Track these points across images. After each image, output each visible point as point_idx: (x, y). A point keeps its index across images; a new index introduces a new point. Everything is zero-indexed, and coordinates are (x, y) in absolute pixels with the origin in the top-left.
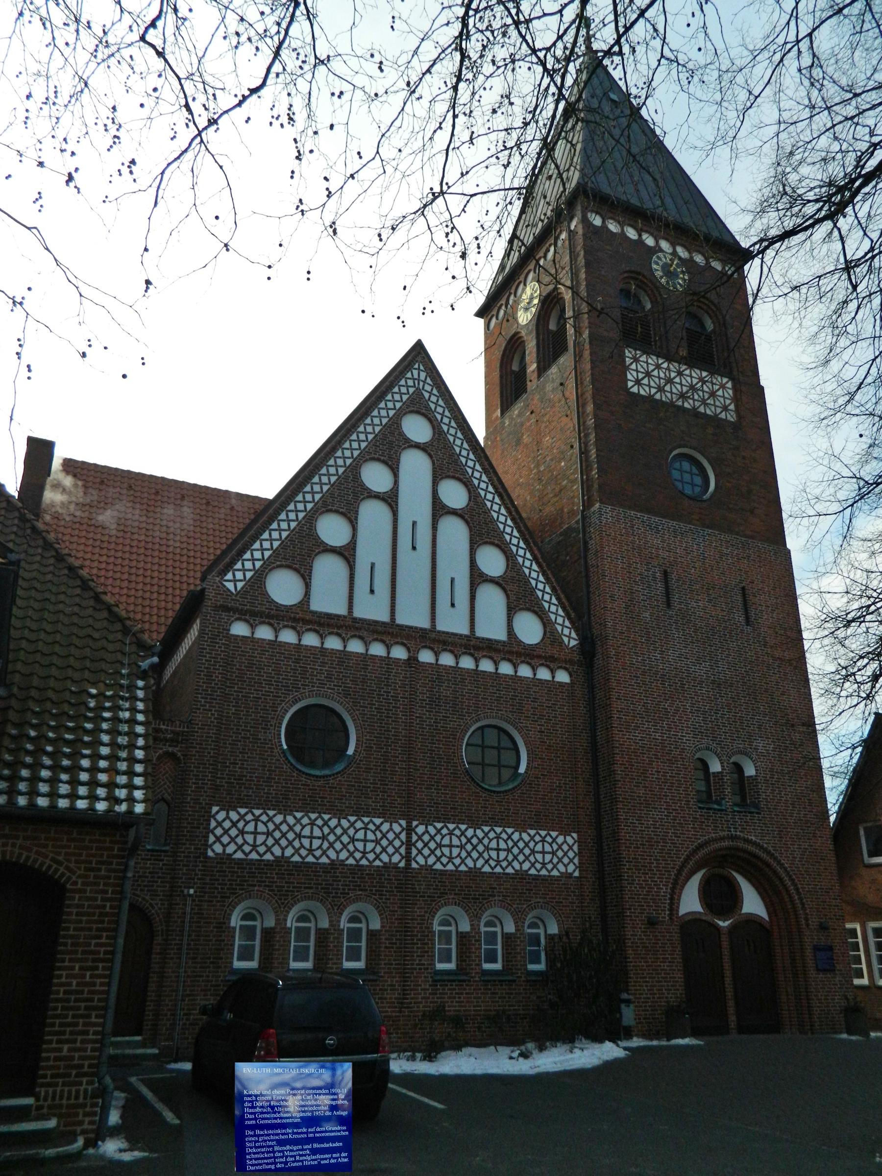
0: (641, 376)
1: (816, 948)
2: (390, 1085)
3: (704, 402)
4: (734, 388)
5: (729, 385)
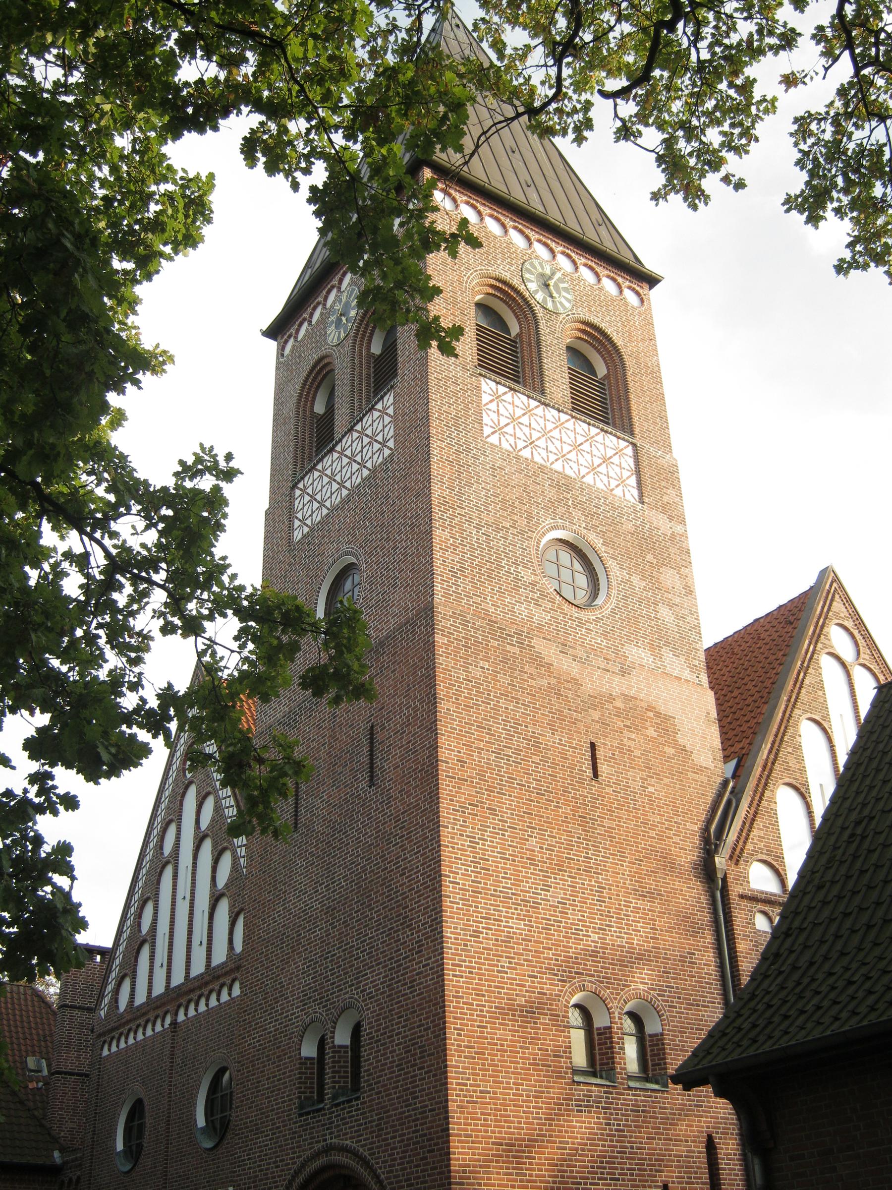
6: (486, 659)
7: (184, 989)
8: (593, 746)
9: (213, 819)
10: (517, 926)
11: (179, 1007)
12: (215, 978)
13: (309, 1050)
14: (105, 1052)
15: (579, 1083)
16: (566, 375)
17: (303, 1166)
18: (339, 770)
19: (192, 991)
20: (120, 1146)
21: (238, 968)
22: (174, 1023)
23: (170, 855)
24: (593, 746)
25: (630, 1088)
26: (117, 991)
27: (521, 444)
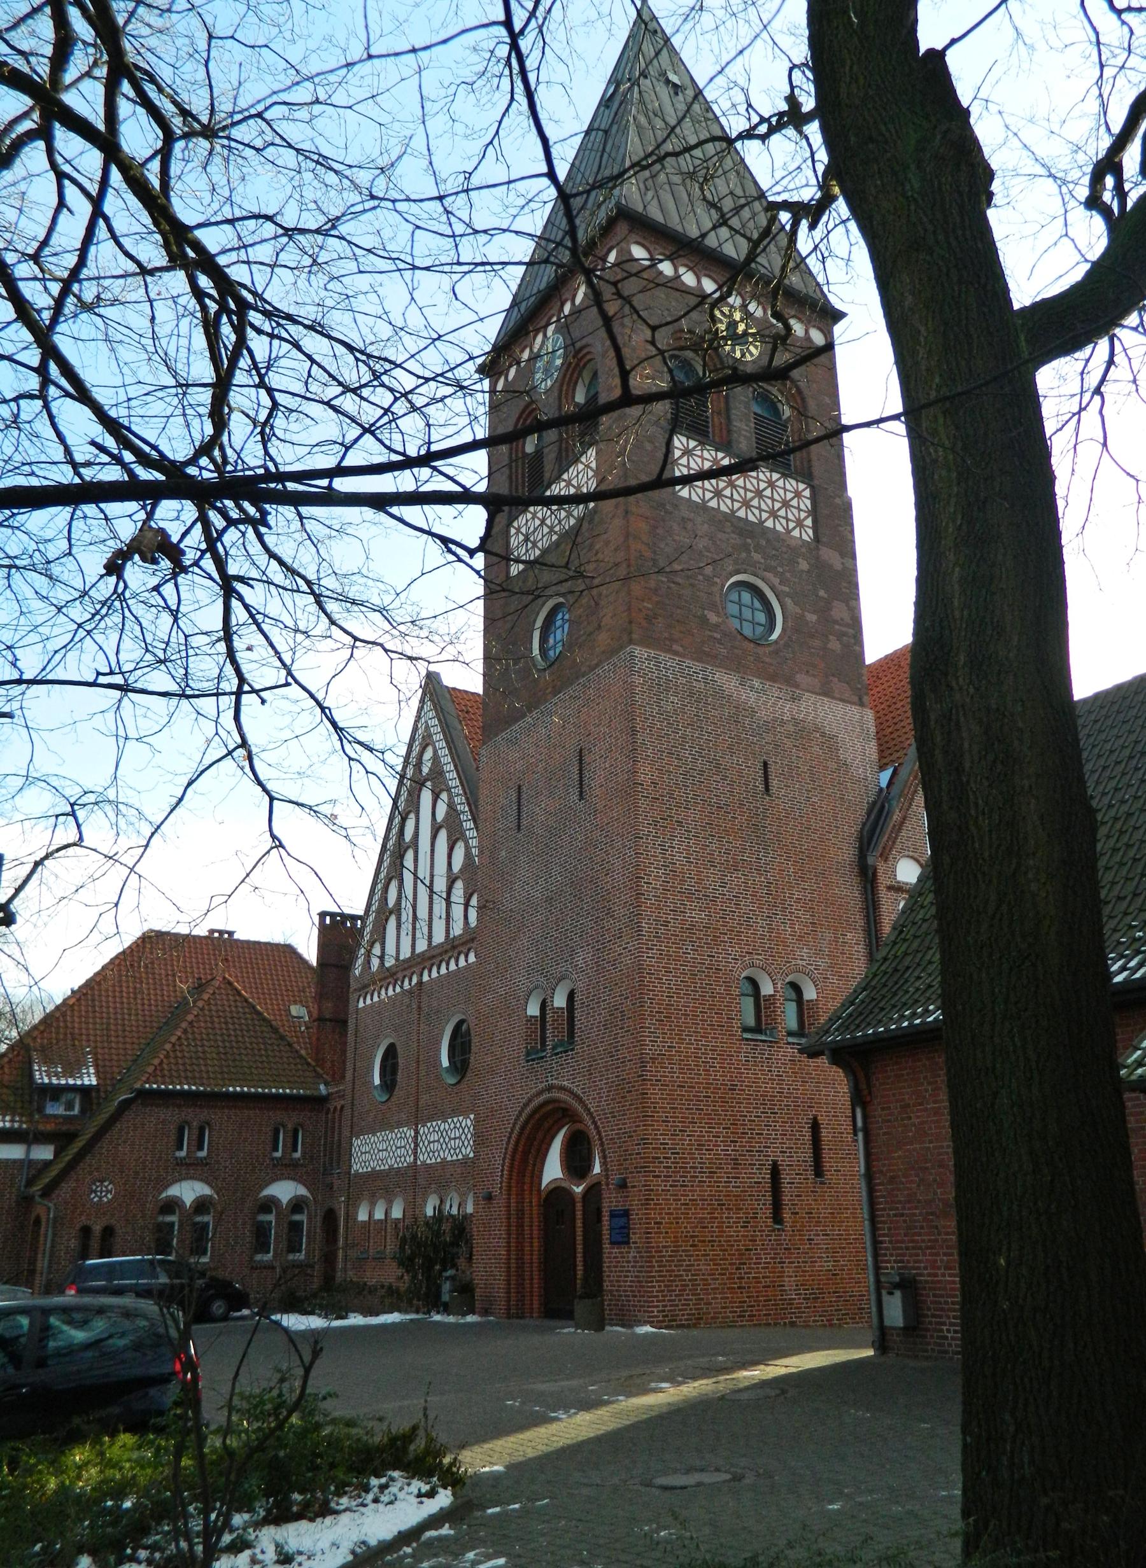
0: (750, 495)
1: (613, 1215)
2: (870, 1352)
3: (773, 514)
4: (813, 498)
5: (807, 493)
6: (676, 694)
7: (428, 955)
8: (765, 764)
9: (447, 813)
10: (699, 917)
11: (423, 969)
12: (453, 947)
13: (533, 1010)
14: (361, 1005)
15: (747, 1040)
16: (753, 425)
17: (530, 1101)
18: (554, 783)
19: (434, 957)
20: (377, 1081)
21: (473, 940)
22: (420, 983)
23: (411, 841)
24: (765, 764)
25: (789, 1043)
26: (369, 953)
27: (708, 495)
